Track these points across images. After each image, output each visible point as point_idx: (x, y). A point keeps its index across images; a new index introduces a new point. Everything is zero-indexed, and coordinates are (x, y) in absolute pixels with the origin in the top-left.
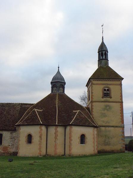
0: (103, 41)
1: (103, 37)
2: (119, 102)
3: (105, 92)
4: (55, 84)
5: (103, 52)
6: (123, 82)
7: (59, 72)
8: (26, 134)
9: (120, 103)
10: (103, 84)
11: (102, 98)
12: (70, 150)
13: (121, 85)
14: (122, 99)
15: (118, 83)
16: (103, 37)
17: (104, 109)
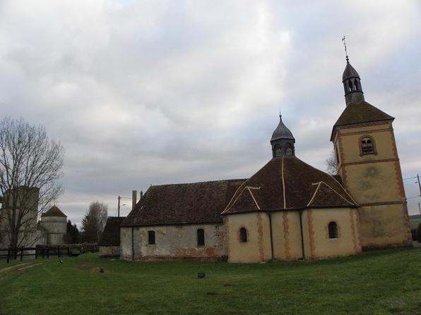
0: (348, 62)
1: (347, 57)
3: (365, 145)
5: (351, 80)
6: (394, 124)
7: (281, 123)
8: (326, 223)
9: (394, 162)
10: (360, 133)
11: (361, 155)
13: (391, 129)
14: (396, 154)
15: (386, 126)
16: (347, 57)
17: (367, 175)
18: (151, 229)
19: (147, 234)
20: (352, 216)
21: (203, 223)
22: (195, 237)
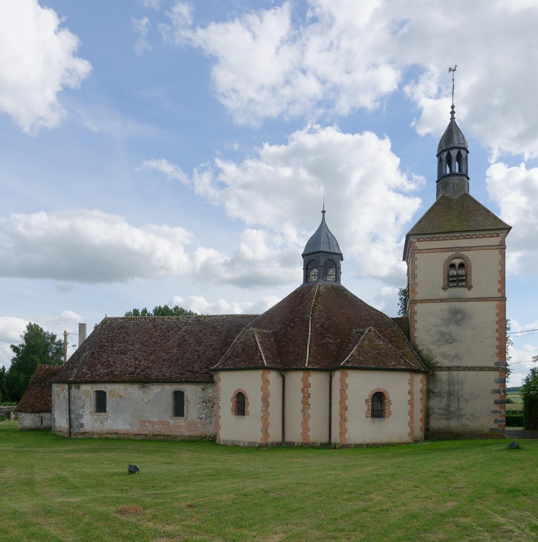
2: (493, 299)
3: (453, 272)
4: (311, 257)
7: (323, 226)
8: (367, 394)
9: (496, 303)
10: (442, 250)
11: (444, 289)
12: (342, 434)
14: (502, 289)
15: (496, 241)
16: (453, 107)
17: (447, 322)
18: (101, 387)
19: (93, 397)
20: (412, 385)
21: (181, 382)
22: (170, 400)
